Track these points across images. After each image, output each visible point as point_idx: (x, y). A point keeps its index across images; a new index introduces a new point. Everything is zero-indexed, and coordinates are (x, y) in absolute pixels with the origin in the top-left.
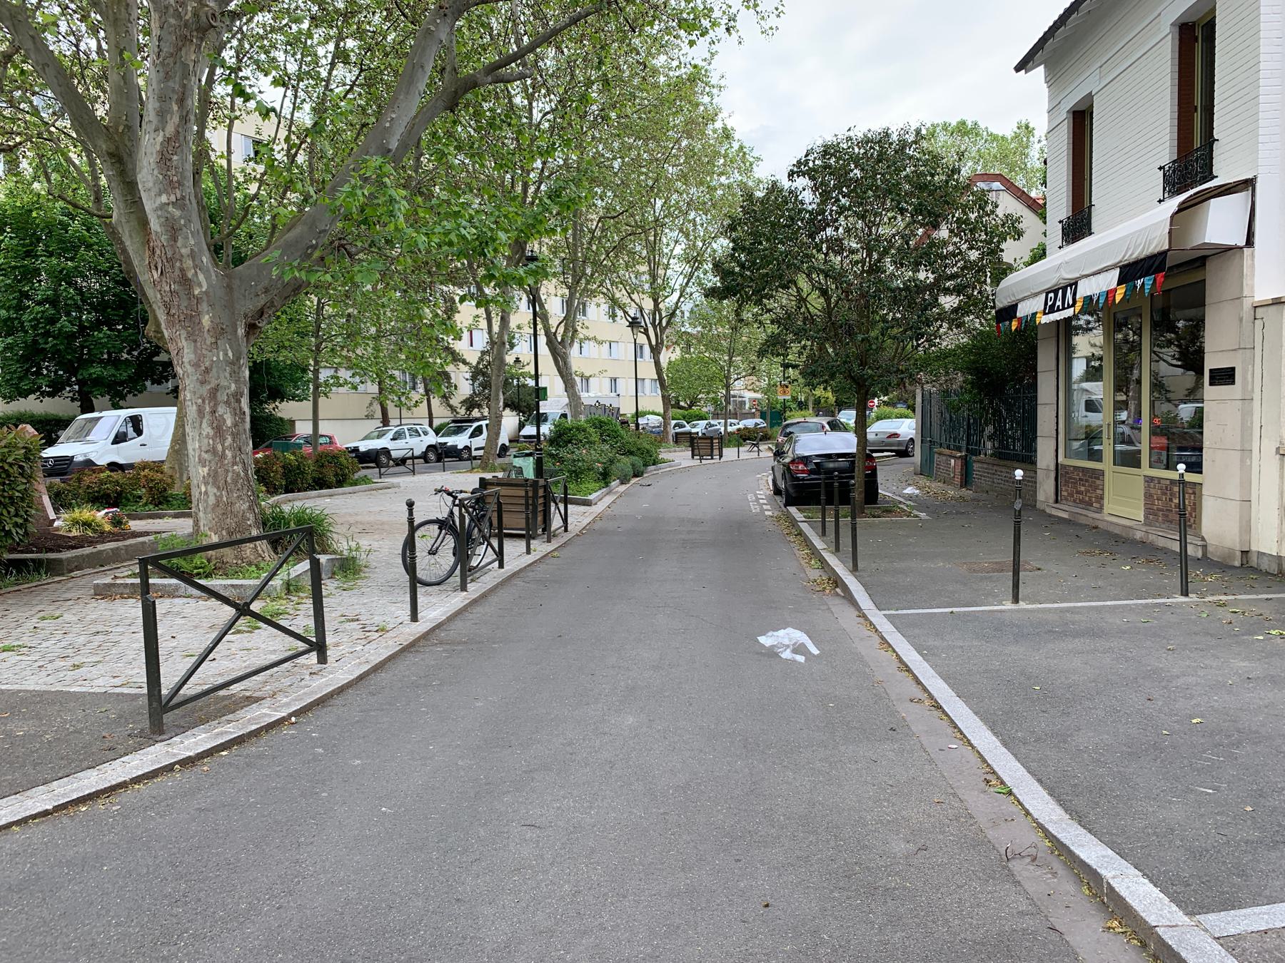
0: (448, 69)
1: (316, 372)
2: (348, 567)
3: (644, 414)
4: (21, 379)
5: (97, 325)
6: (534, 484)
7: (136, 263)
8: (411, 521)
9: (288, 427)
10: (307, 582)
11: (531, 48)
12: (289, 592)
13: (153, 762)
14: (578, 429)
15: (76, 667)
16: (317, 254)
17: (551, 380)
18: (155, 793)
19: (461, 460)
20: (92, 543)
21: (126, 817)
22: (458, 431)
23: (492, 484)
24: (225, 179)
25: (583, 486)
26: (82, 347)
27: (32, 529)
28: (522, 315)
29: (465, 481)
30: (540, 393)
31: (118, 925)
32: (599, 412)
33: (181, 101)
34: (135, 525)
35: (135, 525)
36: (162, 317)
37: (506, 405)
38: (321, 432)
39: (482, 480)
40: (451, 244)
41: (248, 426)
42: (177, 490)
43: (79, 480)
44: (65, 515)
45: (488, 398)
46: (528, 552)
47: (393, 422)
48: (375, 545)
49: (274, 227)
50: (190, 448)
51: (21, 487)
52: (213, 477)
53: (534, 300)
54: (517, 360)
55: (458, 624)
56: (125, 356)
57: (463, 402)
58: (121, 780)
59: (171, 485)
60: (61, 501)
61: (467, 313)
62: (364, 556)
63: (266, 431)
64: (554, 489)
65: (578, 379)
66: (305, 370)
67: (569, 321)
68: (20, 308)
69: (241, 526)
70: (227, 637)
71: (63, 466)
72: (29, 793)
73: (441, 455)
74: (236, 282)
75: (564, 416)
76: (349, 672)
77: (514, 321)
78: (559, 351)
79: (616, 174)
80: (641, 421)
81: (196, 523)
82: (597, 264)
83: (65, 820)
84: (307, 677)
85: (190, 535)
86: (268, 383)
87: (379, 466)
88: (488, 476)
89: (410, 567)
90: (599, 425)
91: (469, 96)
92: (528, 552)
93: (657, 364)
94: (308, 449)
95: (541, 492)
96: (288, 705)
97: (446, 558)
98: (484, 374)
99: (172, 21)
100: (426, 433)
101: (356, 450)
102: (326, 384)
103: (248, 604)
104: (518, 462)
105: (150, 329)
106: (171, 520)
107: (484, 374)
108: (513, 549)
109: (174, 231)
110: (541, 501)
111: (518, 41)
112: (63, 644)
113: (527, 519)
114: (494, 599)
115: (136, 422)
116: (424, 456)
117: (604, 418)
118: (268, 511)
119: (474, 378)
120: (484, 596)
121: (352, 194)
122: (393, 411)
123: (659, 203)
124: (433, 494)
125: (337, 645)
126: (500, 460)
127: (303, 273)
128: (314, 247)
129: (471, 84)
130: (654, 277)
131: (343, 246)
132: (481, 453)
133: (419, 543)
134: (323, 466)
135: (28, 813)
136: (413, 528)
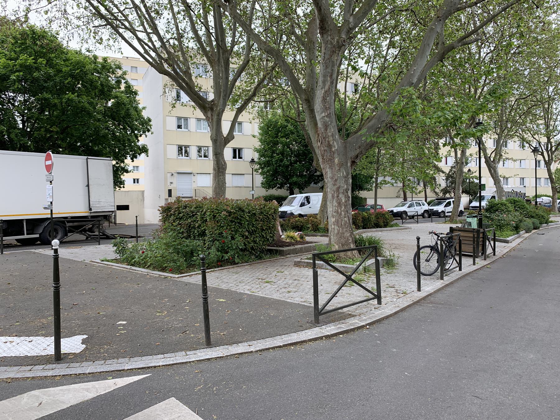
0: (440, 43)
1: (377, 179)
2: (390, 263)
3: (541, 196)
4: (271, 182)
5: (296, 162)
6: (478, 231)
7: (312, 140)
8: (418, 246)
9: (364, 201)
10: (373, 268)
11: (481, 27)
12: (365, 272)
13: (316, 334)
14: (502, 204)
15: (289, 292)
16: (380, 131)
17: (487, 180)
18: (316, 347)
19: (440, 217)
20: (293, 245)
21: (307, 354)
22: (439, 204)
23: (456, 230)
24: (343, 103)
25: (504, 233)
26: (291, 170)
27: (275, 238)
28: (473, 149)
29: (443, 228)
30: (482, 187)
31: (305, 395)
32: (514, 195)
33: (331, 76)
34: (308, 239)
35: (308, 239)
36: (321, 160)
37: (463, 192)
38: (378, 203)
39: (451, 228)
40: (440, 122)
41: (350, 202)
42: (322, 226)
43: (289, 220)
44: (285, 233)
45: (454, 188)
46: (474, 264)
47: (408, 199)
48: (401, 255)
49: (362, 119)
50: (329, 210)
51: (272, 223)
52: (337, 222)
53: (480, 143)
54: (469, 170)
55: (439, 295)
56: (305, 173)
57: (442, 190)
58: (305, 339)
59: (320, 224)
60: (284, 230)
61: (443, 151)
62: (396, 259)
63: (357, 203)
64: (488, 234)
65: (502, 179)
66: (372, 178)
67: (498, 151)
68: (272, 157)
69: (347, 243)
70: (343, 288)
71: (284, 215)
72: (275, 338)
73: (431, 215)
74: (348, 145)
75: (493, 197)
76: (391, 310)
77: (468, 152)
78: (492, 167)
79: (526, 77)
80: (538, 200)
81: (330, 240)
82: (514, 122)
83: (286, 351)
84: (373, 309)
85: (328, 244)
86: (359, 183)
87: (402, 219)
88: (454, 226)
89: (418, 267)
90: (514, 202)
91: (449, 53)
92: (474, 264)
93: (549, 170)
94: (372, 211)
95: (481, 235)
96: (365, 320)
97: (434, 264)
98: (452, 177)
99: (329, 46)
100: (424, 205)
101: (392, 211)
102: (381, 183)
103: (351, 276)
104: (469, 220)
105: (314, 163)
106: (319, 237)
107: (452, 177)
108: (467, 262)
109: (326, 126)
110: (481, 239)
111: (475, 24)
112: (285, 282)
113: (474, 248)
114: (456, 285)
115: (308, 199)
116: (423, 215)
117: (516, 199)
118: (358, 237)
119: (447, 179)
120: (452, 283)
121: (398, 104)
122: (409, 194)
123: (551, 89)
124: (429, 232)
125: (385, 297)
126: (459, 218)
127: (375, 138)
128: (380, 128)
129: (452, 48)
130: (547, 126)
131: (391, 126)
132: (450, 214)
133: (422, 255)
134: (378, 218)
135: (275, 345)
136: (419, 248)
